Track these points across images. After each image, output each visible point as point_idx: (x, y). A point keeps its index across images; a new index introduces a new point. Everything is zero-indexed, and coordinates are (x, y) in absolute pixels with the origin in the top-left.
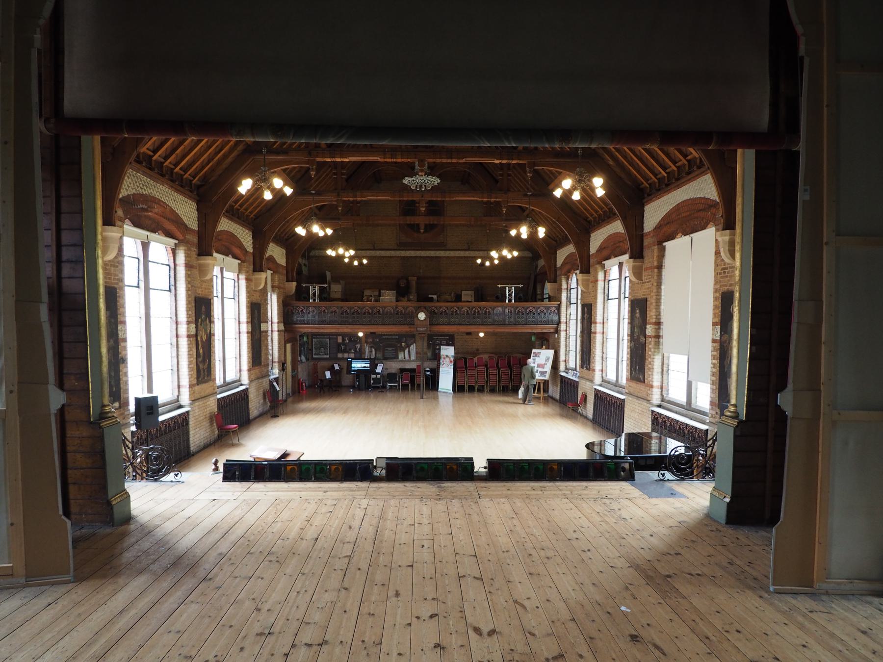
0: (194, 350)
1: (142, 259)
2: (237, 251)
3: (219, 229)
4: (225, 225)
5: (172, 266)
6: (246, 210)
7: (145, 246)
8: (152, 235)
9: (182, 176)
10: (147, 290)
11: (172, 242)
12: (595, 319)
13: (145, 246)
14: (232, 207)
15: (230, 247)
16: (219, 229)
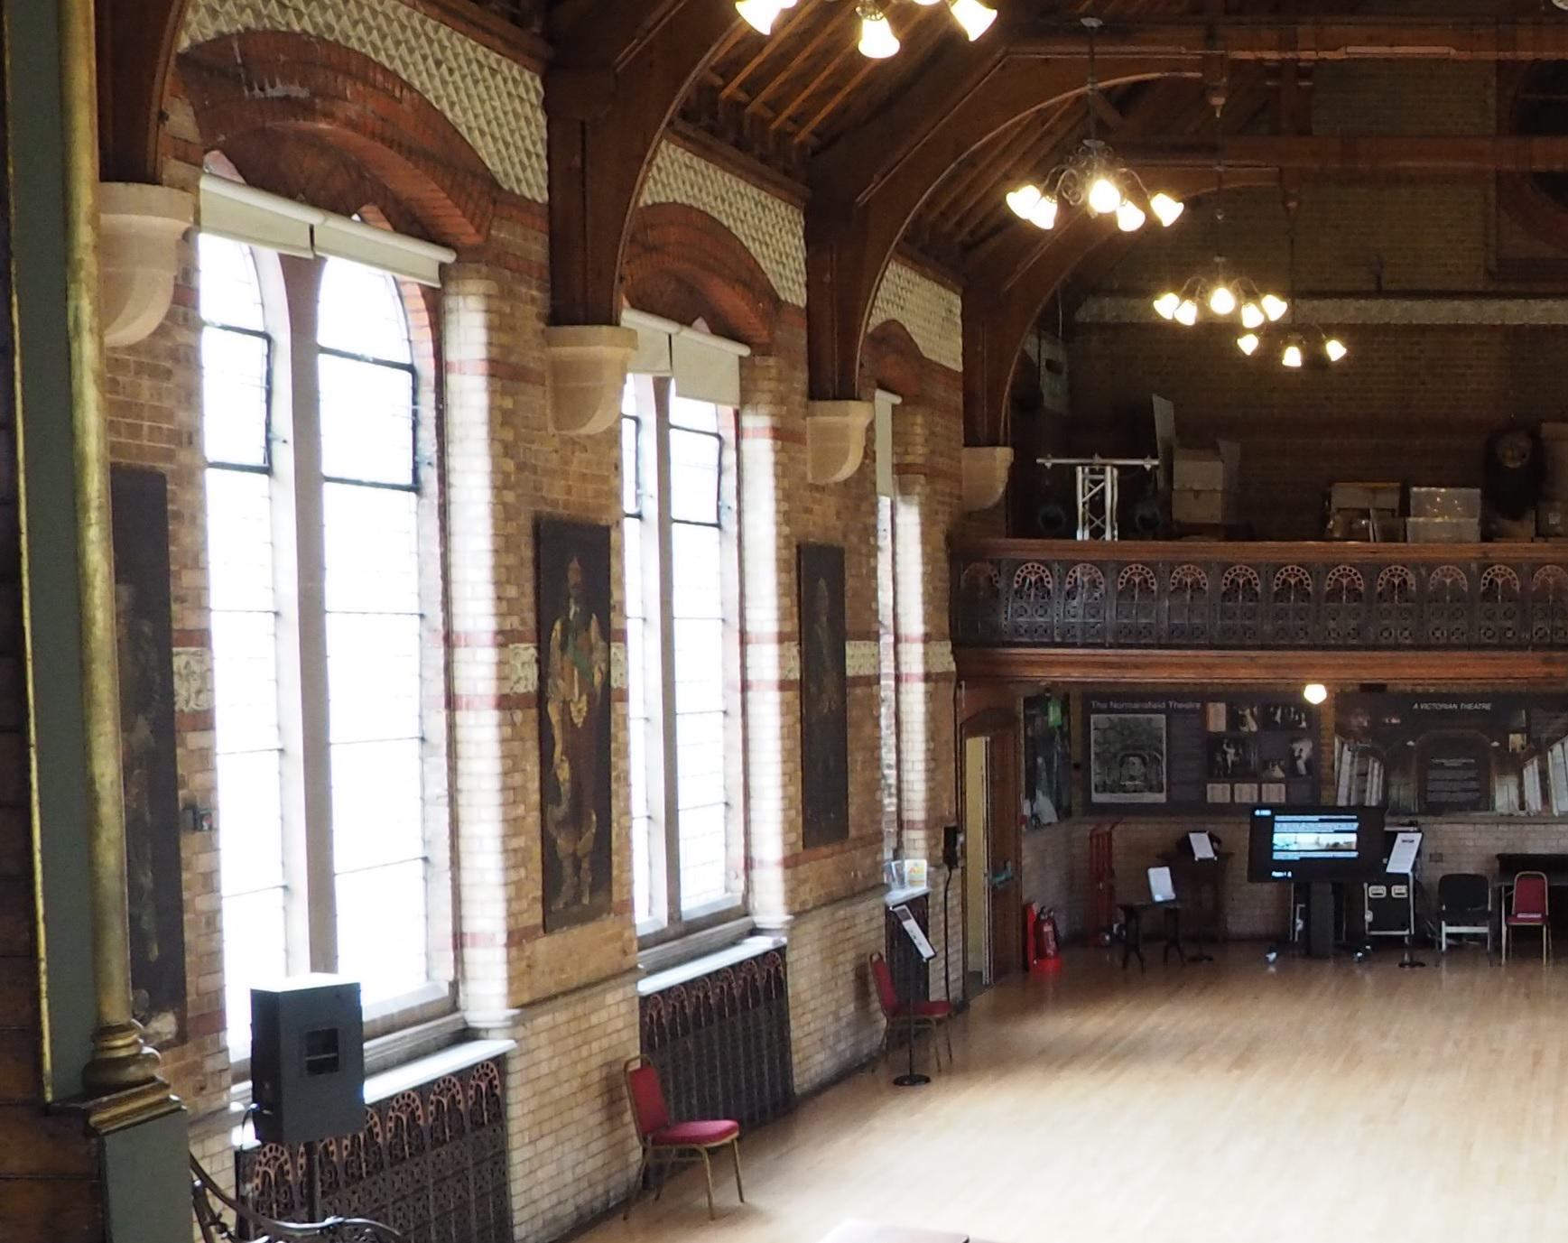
0: (532, 766)
1: (283, 338)
2: (731, 300)
3: (646, 199)
4: (676, 177)
5: (427, 369)
6: (776, 105)
7: (301, 277)
8: (332, 227)
9: (765, 123)
10: (666, 521)
11: (429, 257)
12: (785, 707)
13: (301, 277)
14: (707, 92)
15: (703, 280)
16: (646, 199)
